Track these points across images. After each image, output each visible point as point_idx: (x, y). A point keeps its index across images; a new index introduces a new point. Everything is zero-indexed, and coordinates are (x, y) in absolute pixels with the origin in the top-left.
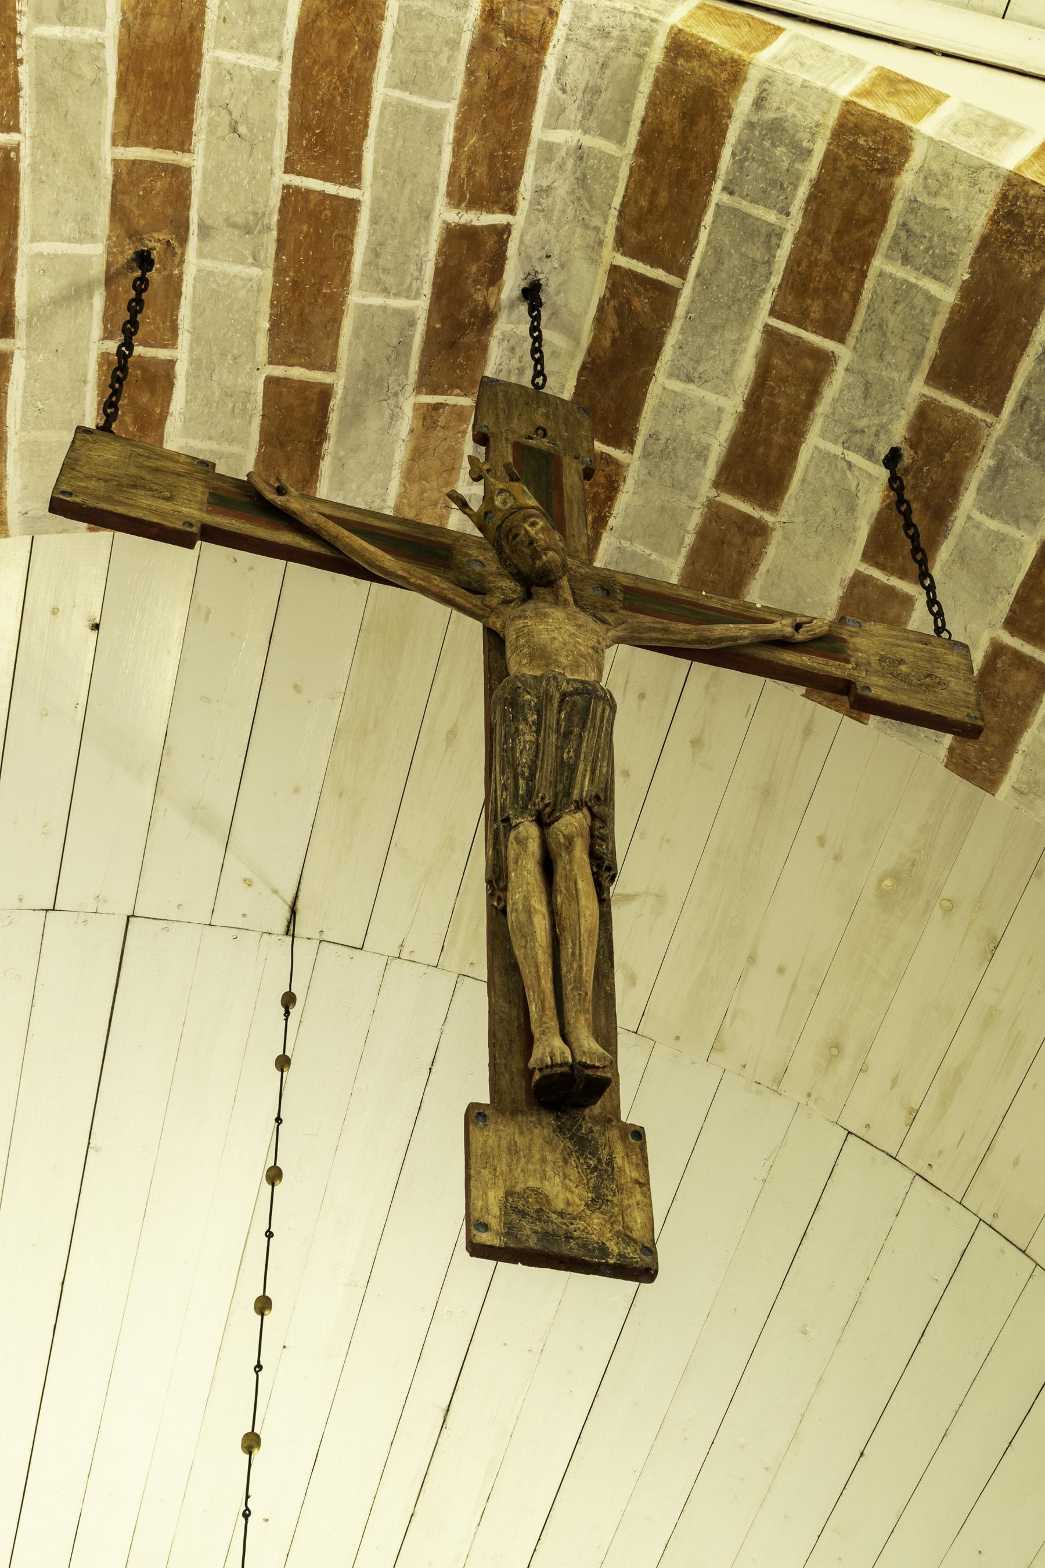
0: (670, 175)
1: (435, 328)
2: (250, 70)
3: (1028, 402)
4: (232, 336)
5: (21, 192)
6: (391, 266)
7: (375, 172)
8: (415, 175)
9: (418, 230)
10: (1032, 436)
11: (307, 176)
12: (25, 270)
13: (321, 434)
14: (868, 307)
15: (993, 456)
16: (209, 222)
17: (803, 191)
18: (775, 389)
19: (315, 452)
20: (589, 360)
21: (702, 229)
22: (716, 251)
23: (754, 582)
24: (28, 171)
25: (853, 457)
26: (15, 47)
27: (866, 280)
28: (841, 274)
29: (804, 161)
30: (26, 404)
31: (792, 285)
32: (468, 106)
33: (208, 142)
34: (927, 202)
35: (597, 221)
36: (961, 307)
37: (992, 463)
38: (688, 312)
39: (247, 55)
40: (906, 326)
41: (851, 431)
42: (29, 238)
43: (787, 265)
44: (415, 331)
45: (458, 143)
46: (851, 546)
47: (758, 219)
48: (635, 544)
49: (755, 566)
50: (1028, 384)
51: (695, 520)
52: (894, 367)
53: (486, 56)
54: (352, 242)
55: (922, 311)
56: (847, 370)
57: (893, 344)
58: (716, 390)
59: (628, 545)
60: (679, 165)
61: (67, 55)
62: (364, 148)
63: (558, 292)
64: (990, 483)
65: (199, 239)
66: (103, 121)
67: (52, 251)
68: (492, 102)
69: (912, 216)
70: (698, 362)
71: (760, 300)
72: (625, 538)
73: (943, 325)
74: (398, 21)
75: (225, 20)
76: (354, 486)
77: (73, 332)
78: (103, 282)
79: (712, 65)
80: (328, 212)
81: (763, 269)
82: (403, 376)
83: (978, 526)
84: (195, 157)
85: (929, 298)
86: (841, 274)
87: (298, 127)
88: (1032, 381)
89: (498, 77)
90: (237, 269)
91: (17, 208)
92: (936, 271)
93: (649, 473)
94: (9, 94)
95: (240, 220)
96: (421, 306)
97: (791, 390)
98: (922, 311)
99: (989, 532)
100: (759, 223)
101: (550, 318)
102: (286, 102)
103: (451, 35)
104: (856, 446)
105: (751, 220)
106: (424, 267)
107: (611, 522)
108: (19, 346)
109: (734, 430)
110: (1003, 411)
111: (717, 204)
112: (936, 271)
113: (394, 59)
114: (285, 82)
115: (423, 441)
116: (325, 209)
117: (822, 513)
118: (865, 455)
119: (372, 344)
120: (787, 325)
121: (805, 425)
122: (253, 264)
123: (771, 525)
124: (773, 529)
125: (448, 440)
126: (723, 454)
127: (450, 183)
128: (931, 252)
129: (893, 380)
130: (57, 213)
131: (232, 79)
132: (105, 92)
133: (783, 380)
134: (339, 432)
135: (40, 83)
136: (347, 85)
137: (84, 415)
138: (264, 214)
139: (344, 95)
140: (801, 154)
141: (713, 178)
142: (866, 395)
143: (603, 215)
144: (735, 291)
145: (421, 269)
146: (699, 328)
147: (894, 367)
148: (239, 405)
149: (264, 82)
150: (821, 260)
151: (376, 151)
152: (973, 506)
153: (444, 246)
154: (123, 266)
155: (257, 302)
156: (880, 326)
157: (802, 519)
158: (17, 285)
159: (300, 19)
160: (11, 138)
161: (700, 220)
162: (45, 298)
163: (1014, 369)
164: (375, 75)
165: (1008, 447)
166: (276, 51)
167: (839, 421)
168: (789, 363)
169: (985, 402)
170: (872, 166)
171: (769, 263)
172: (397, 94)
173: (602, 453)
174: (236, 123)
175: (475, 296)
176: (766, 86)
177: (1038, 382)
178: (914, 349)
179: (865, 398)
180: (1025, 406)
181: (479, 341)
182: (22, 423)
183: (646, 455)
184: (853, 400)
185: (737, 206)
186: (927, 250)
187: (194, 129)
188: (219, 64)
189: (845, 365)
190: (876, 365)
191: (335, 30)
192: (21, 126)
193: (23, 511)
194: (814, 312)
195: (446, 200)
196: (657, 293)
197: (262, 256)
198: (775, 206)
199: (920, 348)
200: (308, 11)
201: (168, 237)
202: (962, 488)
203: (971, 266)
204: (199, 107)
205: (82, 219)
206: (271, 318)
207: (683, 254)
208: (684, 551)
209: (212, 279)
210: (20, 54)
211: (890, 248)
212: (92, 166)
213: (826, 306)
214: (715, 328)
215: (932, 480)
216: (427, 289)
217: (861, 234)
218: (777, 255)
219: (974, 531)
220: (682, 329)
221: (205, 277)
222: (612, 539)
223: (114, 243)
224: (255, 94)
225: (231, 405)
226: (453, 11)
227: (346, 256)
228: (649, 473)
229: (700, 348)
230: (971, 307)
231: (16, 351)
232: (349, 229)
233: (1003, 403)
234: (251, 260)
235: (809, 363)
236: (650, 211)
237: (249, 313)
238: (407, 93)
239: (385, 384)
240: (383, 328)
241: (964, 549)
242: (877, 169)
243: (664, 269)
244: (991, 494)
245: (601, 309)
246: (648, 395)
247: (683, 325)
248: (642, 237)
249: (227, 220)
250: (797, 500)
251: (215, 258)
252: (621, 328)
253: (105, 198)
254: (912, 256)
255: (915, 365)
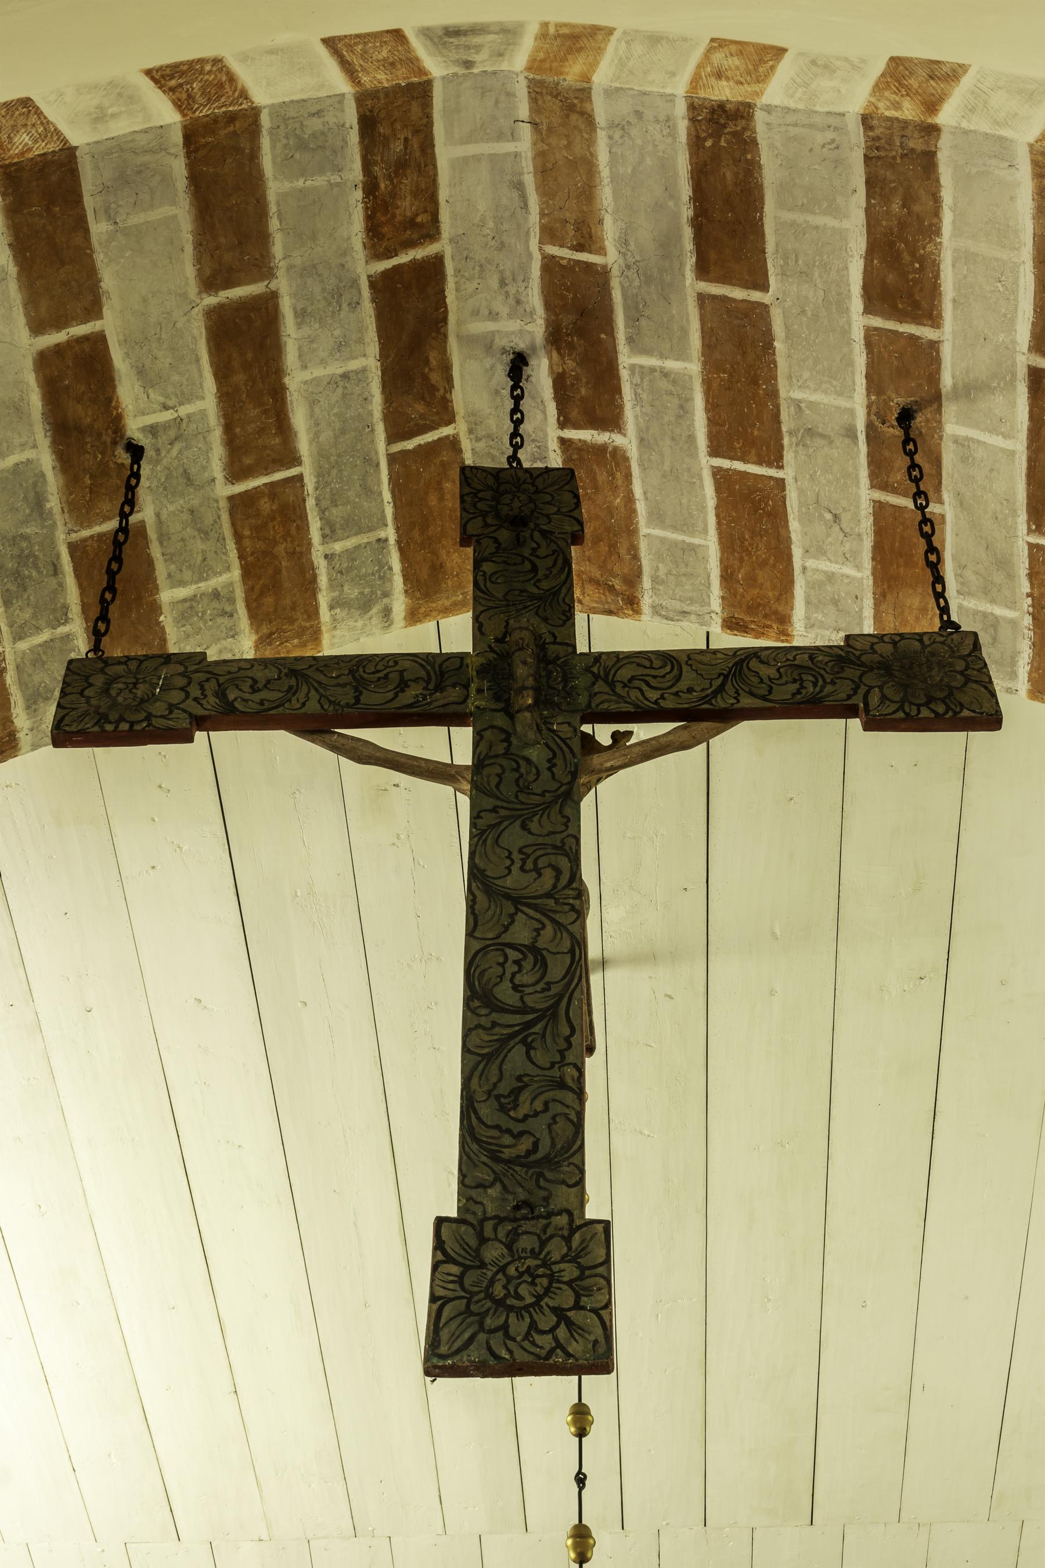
0: (435, 520)
1: (606, 334)
2: (829, 560)
3: (51, 572)
4: (810, 334)
5: (1025, 495)
6: (665, 397)
7: (701, 479)
8: (664, 476)
9: (648, 429)
10: (30, 551)
11: (762, 476)
12: (1019, 427)
13: (700, 223)
14: (224, 539)
15: (50, 512)
16: (847, 441)
17: (323, 580)
18: (265, 418)
19: (701, 206)
20: (442, 330)
21: (390, 500)
22: (370, 492)
23: (190, 229)
24: (1019, 512)
25: (168, 416)
26: (1033, 606)
27: (237, 556)
28: (260, 545)
29: (333, 600)
30: (1015, 292)
31: (295, 509)
32: (631, 531)
33: (858, 507)
34: (224, 642)
35: (481, 445)
36: (152, 595)
37: (48, 506)
38: (373, 430)
39: (834, 570)
40: (186, 551)
41: (181, 435)
42: (1017, 456)
43: (307, 519)
44: (626, 332)
45: (630, 499)
46: (121, 337)
47: (348, 537)
48: (326, 183)
49: (198, 245)
50: (61, 585)
51: (277, 249)
52: (177, 512)
53: (626, 571)
54: (709, 419)
55: (181, 570)
56: (213, 480)
57: (188, 529)
58: (316, 381)
59: (332, 178)
60: (431, 531)
61: (989, 591)
62: (715, 499)
63: (492, 367)
64: (38, 489)
65: (855, 426)
66: (954, 535)
67: (994, 437)
68: (609, 532)
69: (229, 625)
70: (344, 395)
71: (316, 480)
72: (338, 184)
73: (157, 573)
74: (709, 596)
75: (857, 597)
76: (648, 161)
77: (970, 355)
78: (943, 397)
79: (435, 610)
80: (738, 446)
81: (325, 504)
82: (626, 286)
83: (23, 446)
84: (868, 497)
85: (182, 583)
86: (260, 545)
87: (778, 516)
88: (60, 589)
89: (610, 553)
90: (815, 397)
91: (1029, 484)
92: (188, 604)
93: (343, 266)
94: (1037, 573)
95: (820, 442)
96: (626, 359)
97: (251, 428)
98: (181, 570)
99: (10, 451)
100: (346, 535)
101: (492, 342)
102: (793, 536)
103: (661, 588)
104: (170, 426)
105: (353, 532)
106: (633, 396)
107: (359, 194)
108: (1023, 358)
109: (283, 358)
110: (67, 551)
111: (387, 526)
112: (188, 604)
113: (706, 568)
114: (797, 552)
115: (585, 208)
116: (740, 448)
117: (165, 346)
118: (157, 426)
119: (665, 320)
120: (283, 477)
121: (223, 409)
122: (800, 401)
123: (204, 295)
124: (200, 293)
125: (557, 207)
126: (282, 328)
127: (629, 467)
128: (200, 614)
129: (171, 503)
130: (992, 470)
131: (844, 554)
132: (954, 558)
133: (261, 431)
134: (678, 228)
135: (1011, 576)
136: (741, 546)
137: (953, 266)
138: (797, 445)
139: (742, 539)
140: (337, 603)
141: (399, 542)
142: (186, 473)
143: (477, 453)
144: (340, 471)
145: (635, 394)
146: (357, 424)
147: (177, 512)
148: (791, 263)
149: (816, 550)
150: (282, 544)
151: (704, 496)
152: (38, 460)
153: (619, 413)
154: (926, 408)
155: (790, 366)
156: (206, 533)
157: (179, 325)
158: (1026, 416)
159: (793, 597)
160: (1034, 539)
161: (395, 506)
162: (999, 396)
163: (80, 586)
164: (719, 555)
165: (43, 527)
166: (809, 573)
167: (196, 435)
168: (265, 447)
169: (86, 546)
170: (279, 633)
171: (322, 512)
172: (696, 541)
173: (396, 255)
174: (835, 522)
175: (575, 364)
176: (387, 624)
177: (55, 592)
178: (169, 539)
179: (185, 471)
180: (52, 568)
181: (557, 315)
182: (1018, 272)
183: (355, 283)
184: (194, 461)
185: (370, 534)
186: (204, 613)
187: (872, 518)
188: (857, 566)
189: (217, 482)
190: (192, 502)
191: (761, 589)
192: (1026, 547)
193: (1013, 170)
194: (265, 503)
195: (629, 454)
196: (407, 429)
197: (792, 409)
198: (340, 556)
199: (165, 544)
200: (787, 602)
201: (884, 428)
202: (58, 466)
203: (163, 629)
204: (869, 535)
205: (967, 458)
206: (774, 351)
207: (398, 473)
208: (273, 208)
209: (838, 388)
210: (1029, 601)
211: (233, 592)
212: (961, 502)
213: (258, 515)
214: (343, 432)
215: (88, 452)
216: (624, 374)
217: (261, 583)
218: (319, 522)
219: (23, 440)
220: (372, 415)
221: (846, 392)
222: (351, 177)
223: (935, 431)
224: (821, 542)
225: (800, 262)
226: (664, 604)
227: (711, 406)
228: (343, 266)
229: (348, 407)
230: (144, 601)
231: (1026, 352)
232: (714, 430)
233: (72, 557)
234: (803, 405)
235: (248, 461)
236: (439, 483)
237: (796, 356)
238: (688, 541)
239: (642, 278)
240: (659, 337)
241: (21, 418)
242: (274, 634)
243: (409, 450)
244: (31, 481)
245: (449, 380)
246: (376, 339)
247: (372, 418)
248: (437, 461)
249: (831, 442)
250: (194, 338)
251: (838, 408)
252: (425, 378)
253: (948, 474)
254: (212, 600)
255: (161, 528)
